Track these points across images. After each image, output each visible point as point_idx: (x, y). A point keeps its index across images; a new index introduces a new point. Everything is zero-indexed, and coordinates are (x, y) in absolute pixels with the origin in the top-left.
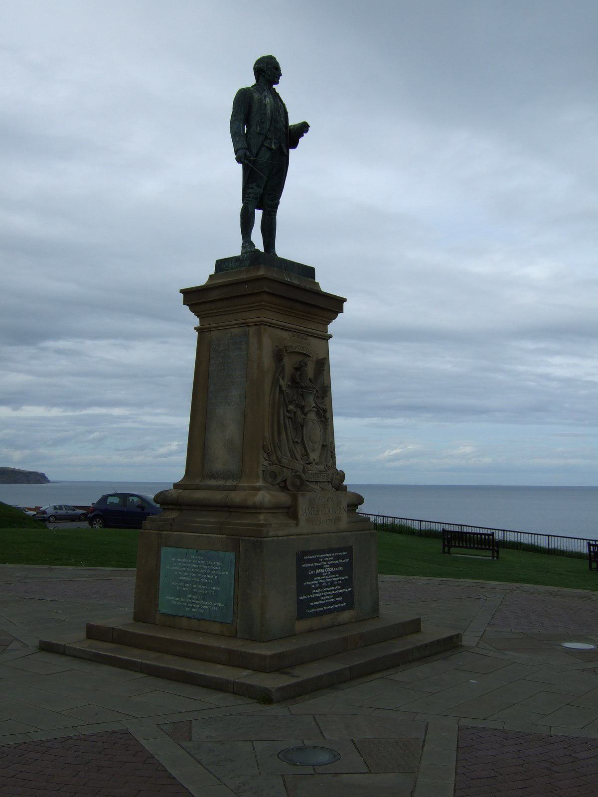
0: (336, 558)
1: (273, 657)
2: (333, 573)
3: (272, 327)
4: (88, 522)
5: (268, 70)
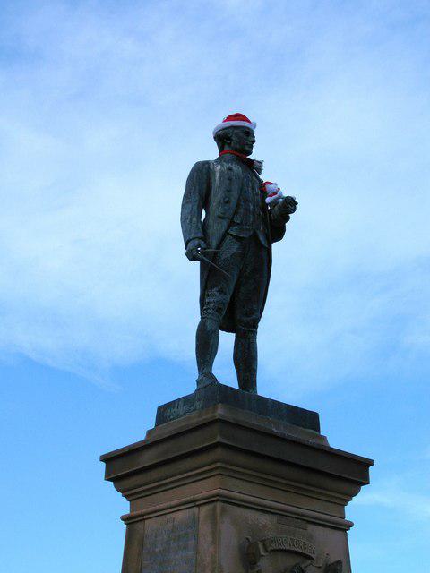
3: (239, 506)
4: (128, 512)
5: (236, 139)
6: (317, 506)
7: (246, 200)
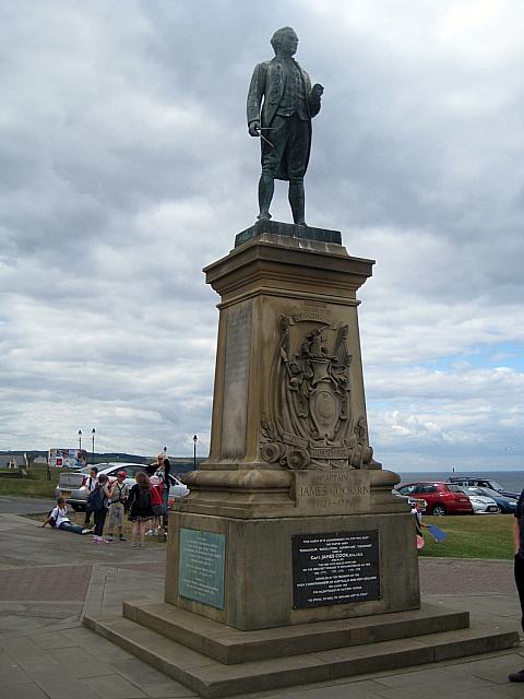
0: (350, 543)
1: (232, 648)
2: (346, 559)
6: (334, 292)
7: (290, 89)
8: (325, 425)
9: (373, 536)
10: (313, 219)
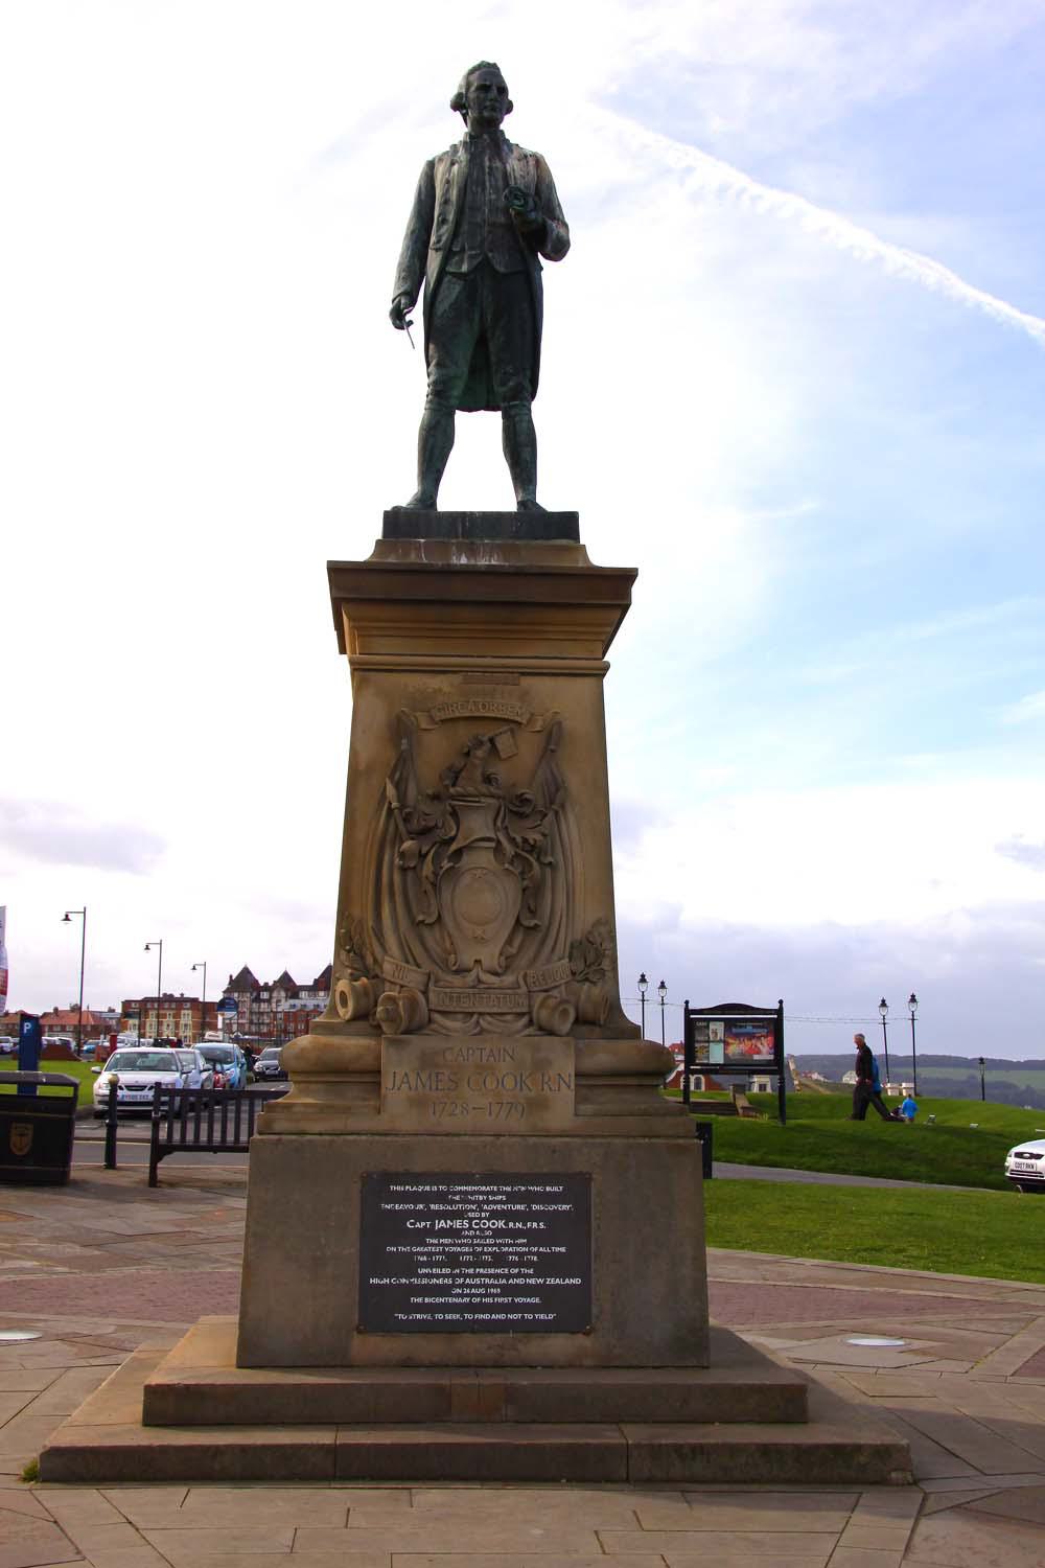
0: (512, 1198)
2: (497, 1233)
6: (542, 649)
8: (481, 941)
9: (578, 1186)
10: (550, 498)
